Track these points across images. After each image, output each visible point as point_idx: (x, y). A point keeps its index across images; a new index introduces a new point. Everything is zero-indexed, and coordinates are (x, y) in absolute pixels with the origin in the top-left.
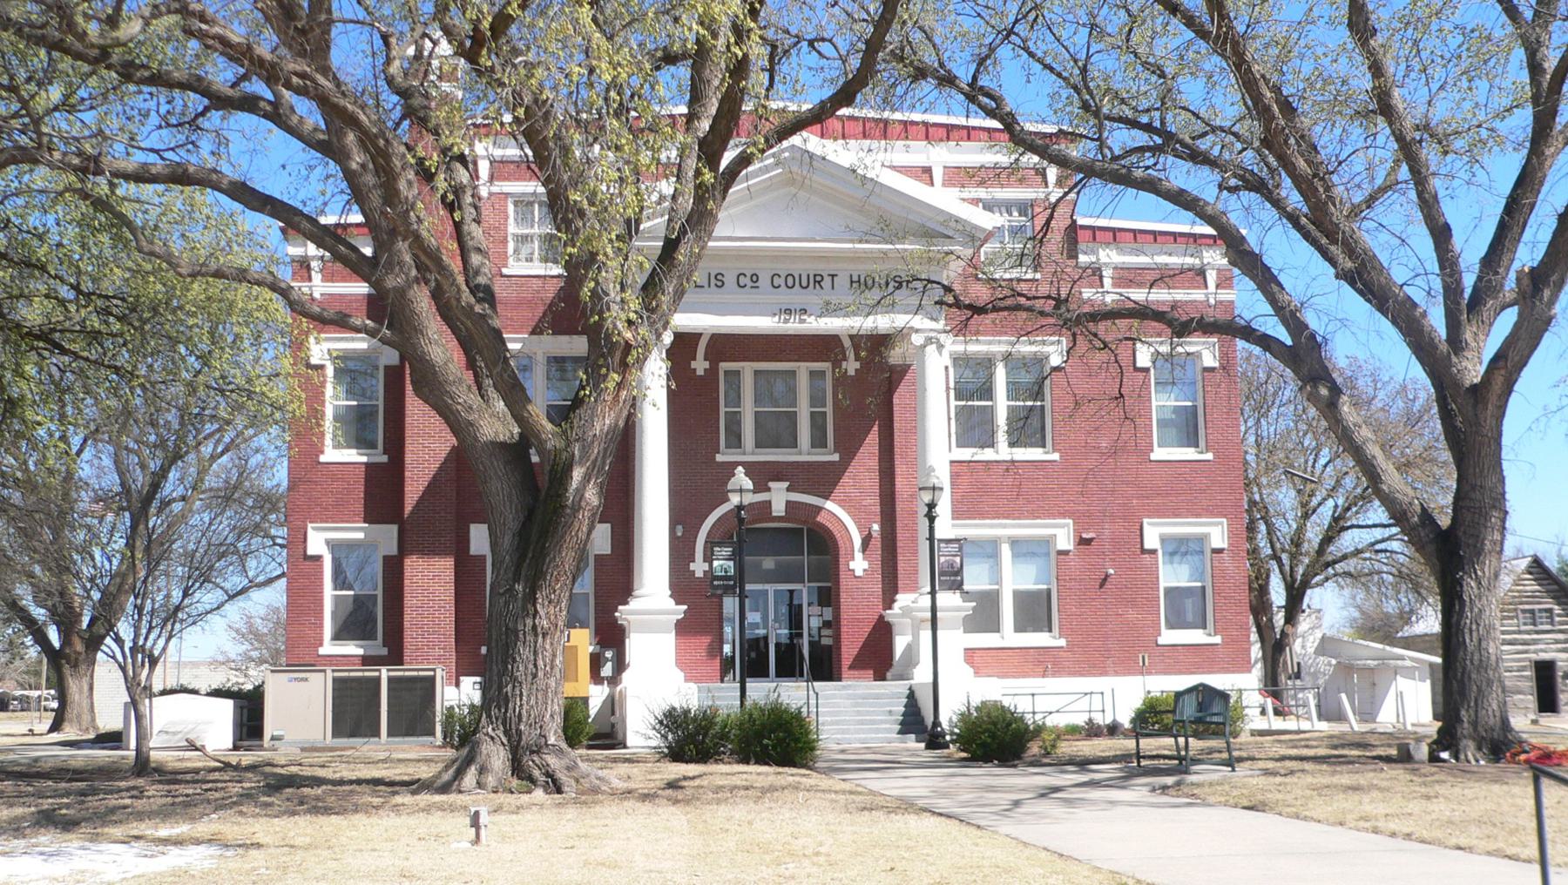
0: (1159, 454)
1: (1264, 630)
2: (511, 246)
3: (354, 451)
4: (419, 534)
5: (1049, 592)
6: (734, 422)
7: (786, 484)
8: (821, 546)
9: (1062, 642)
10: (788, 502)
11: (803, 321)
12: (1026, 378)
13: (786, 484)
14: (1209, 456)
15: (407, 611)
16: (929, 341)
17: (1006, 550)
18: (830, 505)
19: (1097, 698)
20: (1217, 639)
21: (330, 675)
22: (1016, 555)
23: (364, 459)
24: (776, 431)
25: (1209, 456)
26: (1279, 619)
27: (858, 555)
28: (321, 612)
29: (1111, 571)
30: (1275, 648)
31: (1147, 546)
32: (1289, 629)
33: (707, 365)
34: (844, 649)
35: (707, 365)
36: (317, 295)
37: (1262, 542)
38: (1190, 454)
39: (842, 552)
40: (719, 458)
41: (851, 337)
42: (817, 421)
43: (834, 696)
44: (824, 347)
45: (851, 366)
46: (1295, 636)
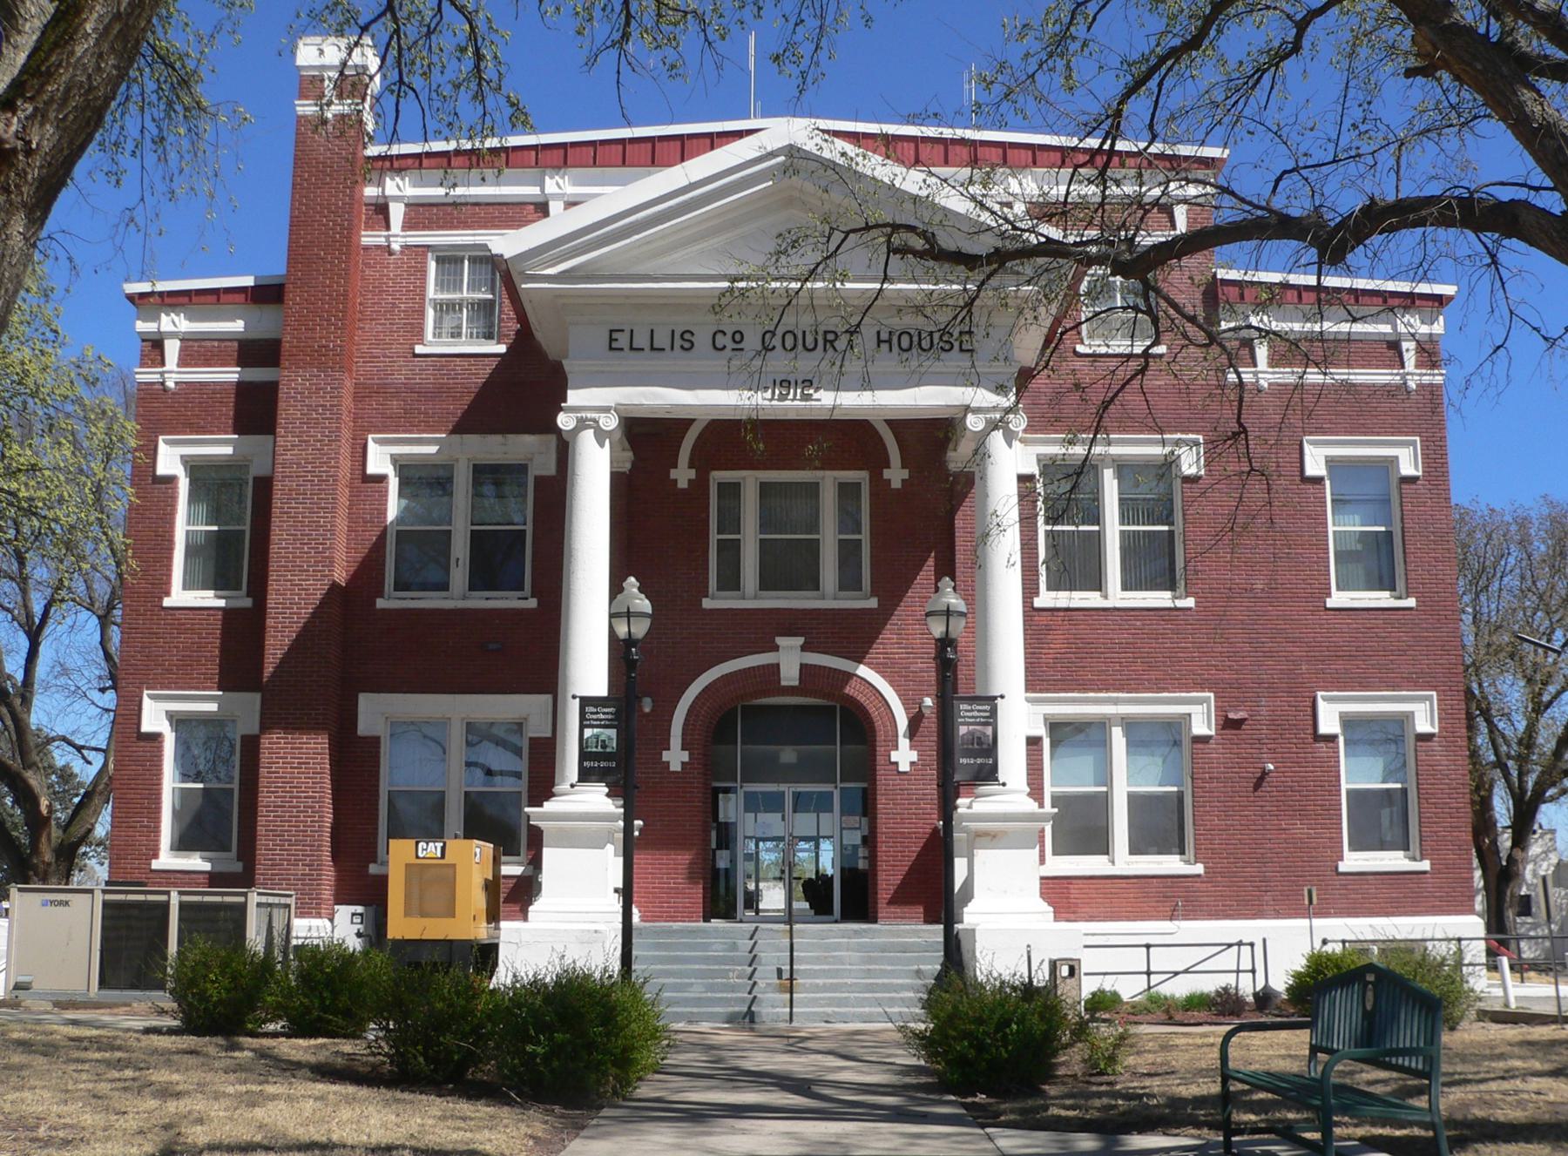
0: (1338, 599)
1: (1487, 856)
2: (430, 314)
3: (211, 593)
4: (284, 710)
5: (1180, 797)
6: (730, 552)
7: (800, 641)
8: (858, 727)
9: (1199, 869)
10: (803, 667)
11: (807, 398)
12: (1148, 489)
13: (800, 641)
14: (1411, 602)
15: (262, 810)
16: (993, 426)
17: (1118, 736)
18: (863, 671)
19: (1246, 950)
20: (1199, 869)
21: (99, 898)
22: (1133, 745)
23: (222, 603)
24: (789, 565)
25: (1411, 602)
26: (1505, 841)
27: (904, 743)
28: (158, 810)
29: (1271, 767)
30: (1501, 877)
31: (1324, 729)
32: (1518, 854)
33: (692, 474)
34: (881, 876)
35: (692, 474)
36: (170, 384)
37: (1482, 740)
38: (1383, 599)
39: (880, 737)
40: (707, 603)
41: (889, 422)
42: (849, 552)
43: (838, 947)
44: (851, 440)
45: (896, 475)
46: (1525, 861)
